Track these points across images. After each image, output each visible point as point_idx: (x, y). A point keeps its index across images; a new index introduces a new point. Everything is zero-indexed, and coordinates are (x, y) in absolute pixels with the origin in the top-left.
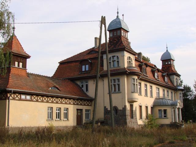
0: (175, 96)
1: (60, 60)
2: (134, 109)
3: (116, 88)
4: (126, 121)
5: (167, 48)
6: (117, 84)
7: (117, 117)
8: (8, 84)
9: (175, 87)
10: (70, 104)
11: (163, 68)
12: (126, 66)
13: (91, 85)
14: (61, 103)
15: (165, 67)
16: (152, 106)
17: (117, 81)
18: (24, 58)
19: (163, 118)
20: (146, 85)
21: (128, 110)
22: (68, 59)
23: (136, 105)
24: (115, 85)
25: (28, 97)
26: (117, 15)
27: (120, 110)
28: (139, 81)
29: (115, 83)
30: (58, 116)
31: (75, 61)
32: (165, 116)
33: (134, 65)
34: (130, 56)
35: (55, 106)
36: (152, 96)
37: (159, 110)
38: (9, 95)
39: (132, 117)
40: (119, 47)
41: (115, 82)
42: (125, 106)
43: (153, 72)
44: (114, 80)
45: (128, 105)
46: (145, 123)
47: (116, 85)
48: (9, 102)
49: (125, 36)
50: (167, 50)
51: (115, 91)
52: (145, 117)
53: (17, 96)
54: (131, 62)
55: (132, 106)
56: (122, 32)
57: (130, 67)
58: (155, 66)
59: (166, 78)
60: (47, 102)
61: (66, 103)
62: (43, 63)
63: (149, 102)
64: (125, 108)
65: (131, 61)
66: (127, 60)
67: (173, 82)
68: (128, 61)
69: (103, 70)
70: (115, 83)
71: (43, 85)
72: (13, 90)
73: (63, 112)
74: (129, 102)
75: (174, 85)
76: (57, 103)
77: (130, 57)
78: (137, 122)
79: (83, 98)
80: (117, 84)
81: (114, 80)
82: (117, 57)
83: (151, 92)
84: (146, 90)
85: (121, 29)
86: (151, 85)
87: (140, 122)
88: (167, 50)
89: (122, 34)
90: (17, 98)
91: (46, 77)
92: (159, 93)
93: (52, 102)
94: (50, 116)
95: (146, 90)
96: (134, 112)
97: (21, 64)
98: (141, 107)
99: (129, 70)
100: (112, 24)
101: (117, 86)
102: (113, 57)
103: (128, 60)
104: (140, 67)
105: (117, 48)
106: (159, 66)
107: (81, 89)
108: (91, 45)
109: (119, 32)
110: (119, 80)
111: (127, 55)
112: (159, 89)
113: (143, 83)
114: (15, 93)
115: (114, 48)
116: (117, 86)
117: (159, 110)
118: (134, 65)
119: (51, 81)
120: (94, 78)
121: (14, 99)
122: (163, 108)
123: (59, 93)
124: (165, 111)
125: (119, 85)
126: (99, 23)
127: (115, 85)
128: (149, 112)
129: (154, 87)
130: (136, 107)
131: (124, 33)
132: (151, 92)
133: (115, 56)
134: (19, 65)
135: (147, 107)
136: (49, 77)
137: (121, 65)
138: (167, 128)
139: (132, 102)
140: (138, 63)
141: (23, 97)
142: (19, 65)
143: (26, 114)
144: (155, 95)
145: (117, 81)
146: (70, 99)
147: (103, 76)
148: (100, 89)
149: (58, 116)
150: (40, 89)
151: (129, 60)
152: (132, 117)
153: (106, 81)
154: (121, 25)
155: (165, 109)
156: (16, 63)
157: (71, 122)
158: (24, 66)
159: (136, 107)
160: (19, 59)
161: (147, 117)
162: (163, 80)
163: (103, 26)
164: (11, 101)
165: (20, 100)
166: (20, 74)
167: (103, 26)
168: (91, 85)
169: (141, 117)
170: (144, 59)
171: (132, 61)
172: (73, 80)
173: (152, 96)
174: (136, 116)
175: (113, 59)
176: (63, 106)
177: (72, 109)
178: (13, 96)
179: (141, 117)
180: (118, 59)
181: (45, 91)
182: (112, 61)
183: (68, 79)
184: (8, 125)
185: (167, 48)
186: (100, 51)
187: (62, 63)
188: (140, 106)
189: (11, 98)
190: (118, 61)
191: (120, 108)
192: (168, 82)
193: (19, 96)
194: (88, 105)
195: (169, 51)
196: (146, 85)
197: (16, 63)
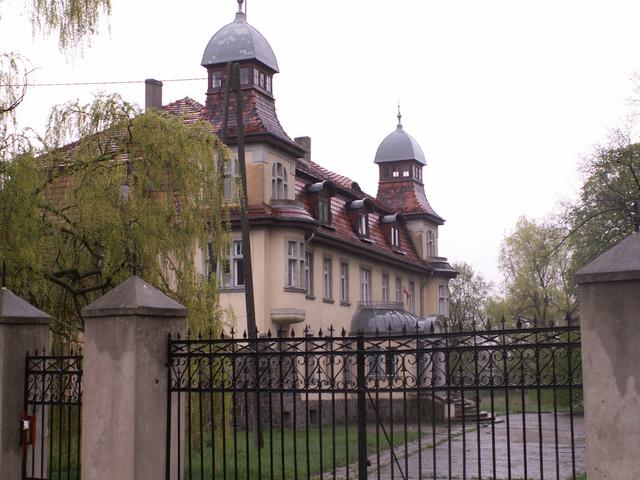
0: (421, 298)
5: (399, 117)
6: (235, 260)
9: (424, 262)
15: (391, 188)
26: (237, 10)
34: (281, 162)
47: (232, 261)
49: (265, 88)
50: (400, 126)
54: (284, 182)
56: (256, 72)
57: (431, 257)
58: (355, 186)
59: (394, 234)
65: (282, 178)
67: (415, 241)
68: (274, 181)
75: (418, 257)
77: (279, 165)
80: (235, 260)
88: (400, 126)
89: (256, 81)
100: (215, 39)
103: (274, 175)
131: (262, 75)
138: (138, 341)
151: (277, 176)
162: (381, 241)
171: (286, 180)
185: (399, 117)
192: (399, 248)
195: (404, 129)
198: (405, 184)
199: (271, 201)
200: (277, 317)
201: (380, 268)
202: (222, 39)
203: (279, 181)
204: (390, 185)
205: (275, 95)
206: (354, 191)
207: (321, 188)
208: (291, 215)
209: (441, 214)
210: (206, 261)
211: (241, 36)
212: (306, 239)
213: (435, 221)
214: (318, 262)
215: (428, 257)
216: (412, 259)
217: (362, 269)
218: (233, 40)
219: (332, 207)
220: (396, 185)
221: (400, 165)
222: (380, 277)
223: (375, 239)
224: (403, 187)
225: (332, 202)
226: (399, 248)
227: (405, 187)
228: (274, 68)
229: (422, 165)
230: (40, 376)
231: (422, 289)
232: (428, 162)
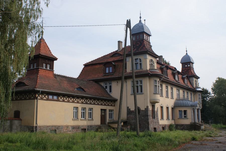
2: (156, 110)
4: (148, 121)
5: (187, 51)
6: (140, 85)
10: (94, 104)
12: (148, 68)
16: (173, 107)
17: (139, 82)
19: (184, 119)
21: (150, 111)
25: (55, 98)
26: (140, 20)
27: (143, 111)
29: (137, 85)
31: (99, 64)
32: (185, 117)
33: (156, 68)
40: (142, 50)
41: (137, 83)
42: (147, 107)
47: (139, 86)
48: (37, 101)
49: (148, 40)
50: (187, 54)
53: (45, 96)
54: (153, 65)
56: (145, 35)
57: (152, 69)
58: (175, 68)
60: (73, 102)
61: (91, 104)
64: (147, 109)
65: (153, 63)
67: (192, 84)
68: (150, 64)
69: (126, 72)
70: (137, 85)
72: (41, 90)
73: (87, 111)
77: (152, 60)
80: (140, 85)
82: (140, 59)
88: (187, 54)
89: (145, 38)
90: (45, 98)
96: (155, 112)
97: (48, 66)
103: (150, 62)
105: (140, 51)
106: (179, 68)
109: (141, 35)
110: (141, 82)
115: (137, 51)
118: (156, 68)
121: (42, 99)
122: (183, 109)
124: (185, 112)
125: (141, 86)
126: (124, 27)
130: (158, 108)
131: (147, 36)
133: (138, 59)
134: (46, 67)
137: (143, 67)
140: (159, 66)
141: (50, 97)
142: (46, 67)
150: (67, 90)
151: (151, 63)
152: (154, 117)
155: (185, 109)
156: (44, 65)
159: (158, 108)
164: (39, 101)
165: (48, 99)
171: (154, 64)
174: (157, 116)
175: (136, 62)
180: (141, 62)
182: (140, 64)
183: (93, 80)
184: (36, 124)
185: (187, 51)
187: (86, 65)
188: (167, 107)
189: (39, 98)
190: (141, 64)
191: (143, 108)
194: (111, 105)
195: (188, 54)
197: (44, 65)
198: (189, 68)
199: (149, 69)
200: (151, 101)
201: (176, 87)
202: (135, 27)
203: (152, 64)
204: (185, 69)
205: (151, 42)
206: (173, 69)
207: (164, 66)
208: (155, 73)
209: (199, 77)
210: (132, 86)
211: (140, 26)
212: (160, 80)
213: (198, 78)
214: (164, 86)
215: (195, 87)
216: (190, 86)
217: (177, 90)
218: (138, 27)
219: (168, 72)
220: (186, 68)
221: (187, 63)
222: (190, 94)
223: (181, 81)
224: (188, 69)
225: (168, 71)
226: (187, 84)
227: (189, 69)
228: (151, 35)
229: (193, 63)
230: (7, 119)
231: (194, 95)
232: (152, 34)
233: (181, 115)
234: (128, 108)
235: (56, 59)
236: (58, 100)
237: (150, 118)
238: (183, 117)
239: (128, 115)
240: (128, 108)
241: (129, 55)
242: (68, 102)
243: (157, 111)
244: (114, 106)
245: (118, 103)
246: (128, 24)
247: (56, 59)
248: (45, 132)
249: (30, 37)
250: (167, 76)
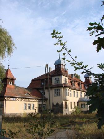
1: (32, 79)
2: (67, 104)
3: (58, 94)
7: (59, 108)
8: (5, 93)
10: (35, 101)
11: (85, 81)
12: (63, 83)
13: (46, 92)
14: (31, 101)
17: (58, 90)
18: (13, 80)
20: (74, 92)
22: (36, 78)
23: (67, 102)
24: (57, 92)
27: (60, 105)
28: (70, 90)
30: (29, 107)
31: (39, 80)
33: (67, 82)
35: (28, 103)
36: (78, 96)
37: (82, 104)
38: (5, 98)
39: (66, 108)
40: (60, 74)
41: (57, 91)
42: (62, 103)
43: (79, 84)
44: (57, 90)
45: (64, 103)
46: (73, 110)
51: (58, 95)
52: (74, 108)
53: (9, 99)
55: (66, 103)
56: (61, 66)
60: (24, 101)
61: (33, 101)
62: (23, 80)
63: (76, 100)
64: (62, 104)
66: (64, 80)
71: (22, 92)
72: (7, 96)
73: (31, 106)
74: (64, 101)
76: (29, 101)
78: (68, 111)
79: (42, 99)
81: (57, 90)
82: (59, 78)
83: (77, 95)
84: (74, 94)
85: (60, 64)
86: (74, 90)
87: (71, 110)
89: (61, 67)
90: (9, 100)
91: (24, 88)
92: (82, 95)
93: (26, 101)
94: (25, 108)
95: (74, 94)
97: (12, 83)
98: (71, 103)
99: (64, 85)
101: (58, 93)
102: (57, 78)
104: (71, 82)
107: (42, 94)
108: (44, 73)
109: (60, 66)
110: (59, 90)
111: (63, 77)
112: (82, 93)
113: (73, 91)
114: (8, 97)
116: (58, 93)
117: (82, 104)
118: (67, 82)
119: (26, 90)
120: (47, 88)
121: (8, 100)
122: (83, 103)
123: (29, 97)
125: (59, 92)
126: (45, 67)
127: (57, 92)
128: (76, 105)
129: (79, 92)
132: (77, 95)
134: (10, 84)
135: (75, 103)
136: (26, 88)
137: (60, 82)
139: (66, 100)
140: (70, 81)
141: (12, 99)
142: (10, 84)
143: (14, 107)
144: (79, 96)
145: (56, 90)
146: (35, 99)
147: (52, 88)
148: (50, 94)
149: (29, 107)
150: (20, 95)
152: (66, 108)
153: (53, 90)
154: (61, 62)
156: (10, 83)
157: (36, 110)
158: (13, 84)
160: (11, 80)
161: (75, 107)
163: (47, 68)
164: (6, 101)
165: (11, 100)
166: (11, 87)
167: (47, 68)
168: (46, 92)
169: (71, 108)
170: (77, 75)
172: (38, 89)
173: (78, 96)
174: (68, 107)
176: (32, 103)
177: (36, 104)
178: (7, 99)
179: (71, 108)
181: (23, 96)
183: (36, 89)
184: (5, 112)
186: (48, 78)
187: (33, 81)
189: (6, 100)
190: (59, 81)
191: (60, 104)
193: (10, 99)
196: (74, 92)
197: (10, 83)
233: (82, 106)
234: (53, 103)
235: (15, 79)
236: (16, 101)
237: (64, 109)
238: (83, 107)
239: (53, 107)
240: (53, 103)
241: (54, 76)
242: (21, 101)
243: (68, 104)
244: (46, 102)
245: (48, 101)
246: (47, 66)
247: (15, 79)
248: (66, 71)
249: (8, 56)
250: (75, 86)
